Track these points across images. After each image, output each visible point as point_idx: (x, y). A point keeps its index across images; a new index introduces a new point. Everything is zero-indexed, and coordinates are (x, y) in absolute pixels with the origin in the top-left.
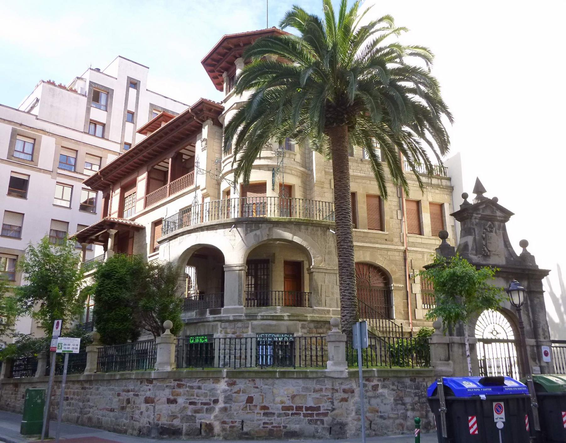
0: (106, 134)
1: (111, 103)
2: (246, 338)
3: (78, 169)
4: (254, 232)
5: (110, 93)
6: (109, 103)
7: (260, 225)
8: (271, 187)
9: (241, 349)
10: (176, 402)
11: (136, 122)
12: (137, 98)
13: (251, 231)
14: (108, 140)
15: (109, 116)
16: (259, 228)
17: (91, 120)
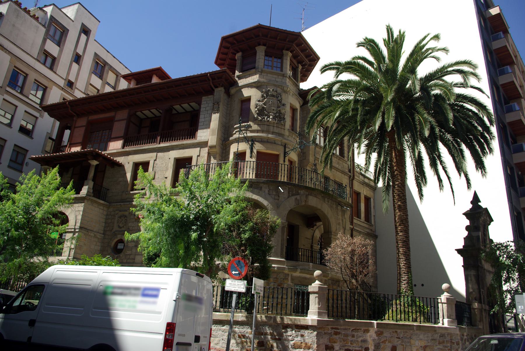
0: (55, 67)
3: (25, 92)
4: (295, 197)
5: (66, 32)
6: (63, 40)
10: (334, 349)
13: (293, 195)
14: (55, 73)
15: (61, 52)
17: (45, 50)
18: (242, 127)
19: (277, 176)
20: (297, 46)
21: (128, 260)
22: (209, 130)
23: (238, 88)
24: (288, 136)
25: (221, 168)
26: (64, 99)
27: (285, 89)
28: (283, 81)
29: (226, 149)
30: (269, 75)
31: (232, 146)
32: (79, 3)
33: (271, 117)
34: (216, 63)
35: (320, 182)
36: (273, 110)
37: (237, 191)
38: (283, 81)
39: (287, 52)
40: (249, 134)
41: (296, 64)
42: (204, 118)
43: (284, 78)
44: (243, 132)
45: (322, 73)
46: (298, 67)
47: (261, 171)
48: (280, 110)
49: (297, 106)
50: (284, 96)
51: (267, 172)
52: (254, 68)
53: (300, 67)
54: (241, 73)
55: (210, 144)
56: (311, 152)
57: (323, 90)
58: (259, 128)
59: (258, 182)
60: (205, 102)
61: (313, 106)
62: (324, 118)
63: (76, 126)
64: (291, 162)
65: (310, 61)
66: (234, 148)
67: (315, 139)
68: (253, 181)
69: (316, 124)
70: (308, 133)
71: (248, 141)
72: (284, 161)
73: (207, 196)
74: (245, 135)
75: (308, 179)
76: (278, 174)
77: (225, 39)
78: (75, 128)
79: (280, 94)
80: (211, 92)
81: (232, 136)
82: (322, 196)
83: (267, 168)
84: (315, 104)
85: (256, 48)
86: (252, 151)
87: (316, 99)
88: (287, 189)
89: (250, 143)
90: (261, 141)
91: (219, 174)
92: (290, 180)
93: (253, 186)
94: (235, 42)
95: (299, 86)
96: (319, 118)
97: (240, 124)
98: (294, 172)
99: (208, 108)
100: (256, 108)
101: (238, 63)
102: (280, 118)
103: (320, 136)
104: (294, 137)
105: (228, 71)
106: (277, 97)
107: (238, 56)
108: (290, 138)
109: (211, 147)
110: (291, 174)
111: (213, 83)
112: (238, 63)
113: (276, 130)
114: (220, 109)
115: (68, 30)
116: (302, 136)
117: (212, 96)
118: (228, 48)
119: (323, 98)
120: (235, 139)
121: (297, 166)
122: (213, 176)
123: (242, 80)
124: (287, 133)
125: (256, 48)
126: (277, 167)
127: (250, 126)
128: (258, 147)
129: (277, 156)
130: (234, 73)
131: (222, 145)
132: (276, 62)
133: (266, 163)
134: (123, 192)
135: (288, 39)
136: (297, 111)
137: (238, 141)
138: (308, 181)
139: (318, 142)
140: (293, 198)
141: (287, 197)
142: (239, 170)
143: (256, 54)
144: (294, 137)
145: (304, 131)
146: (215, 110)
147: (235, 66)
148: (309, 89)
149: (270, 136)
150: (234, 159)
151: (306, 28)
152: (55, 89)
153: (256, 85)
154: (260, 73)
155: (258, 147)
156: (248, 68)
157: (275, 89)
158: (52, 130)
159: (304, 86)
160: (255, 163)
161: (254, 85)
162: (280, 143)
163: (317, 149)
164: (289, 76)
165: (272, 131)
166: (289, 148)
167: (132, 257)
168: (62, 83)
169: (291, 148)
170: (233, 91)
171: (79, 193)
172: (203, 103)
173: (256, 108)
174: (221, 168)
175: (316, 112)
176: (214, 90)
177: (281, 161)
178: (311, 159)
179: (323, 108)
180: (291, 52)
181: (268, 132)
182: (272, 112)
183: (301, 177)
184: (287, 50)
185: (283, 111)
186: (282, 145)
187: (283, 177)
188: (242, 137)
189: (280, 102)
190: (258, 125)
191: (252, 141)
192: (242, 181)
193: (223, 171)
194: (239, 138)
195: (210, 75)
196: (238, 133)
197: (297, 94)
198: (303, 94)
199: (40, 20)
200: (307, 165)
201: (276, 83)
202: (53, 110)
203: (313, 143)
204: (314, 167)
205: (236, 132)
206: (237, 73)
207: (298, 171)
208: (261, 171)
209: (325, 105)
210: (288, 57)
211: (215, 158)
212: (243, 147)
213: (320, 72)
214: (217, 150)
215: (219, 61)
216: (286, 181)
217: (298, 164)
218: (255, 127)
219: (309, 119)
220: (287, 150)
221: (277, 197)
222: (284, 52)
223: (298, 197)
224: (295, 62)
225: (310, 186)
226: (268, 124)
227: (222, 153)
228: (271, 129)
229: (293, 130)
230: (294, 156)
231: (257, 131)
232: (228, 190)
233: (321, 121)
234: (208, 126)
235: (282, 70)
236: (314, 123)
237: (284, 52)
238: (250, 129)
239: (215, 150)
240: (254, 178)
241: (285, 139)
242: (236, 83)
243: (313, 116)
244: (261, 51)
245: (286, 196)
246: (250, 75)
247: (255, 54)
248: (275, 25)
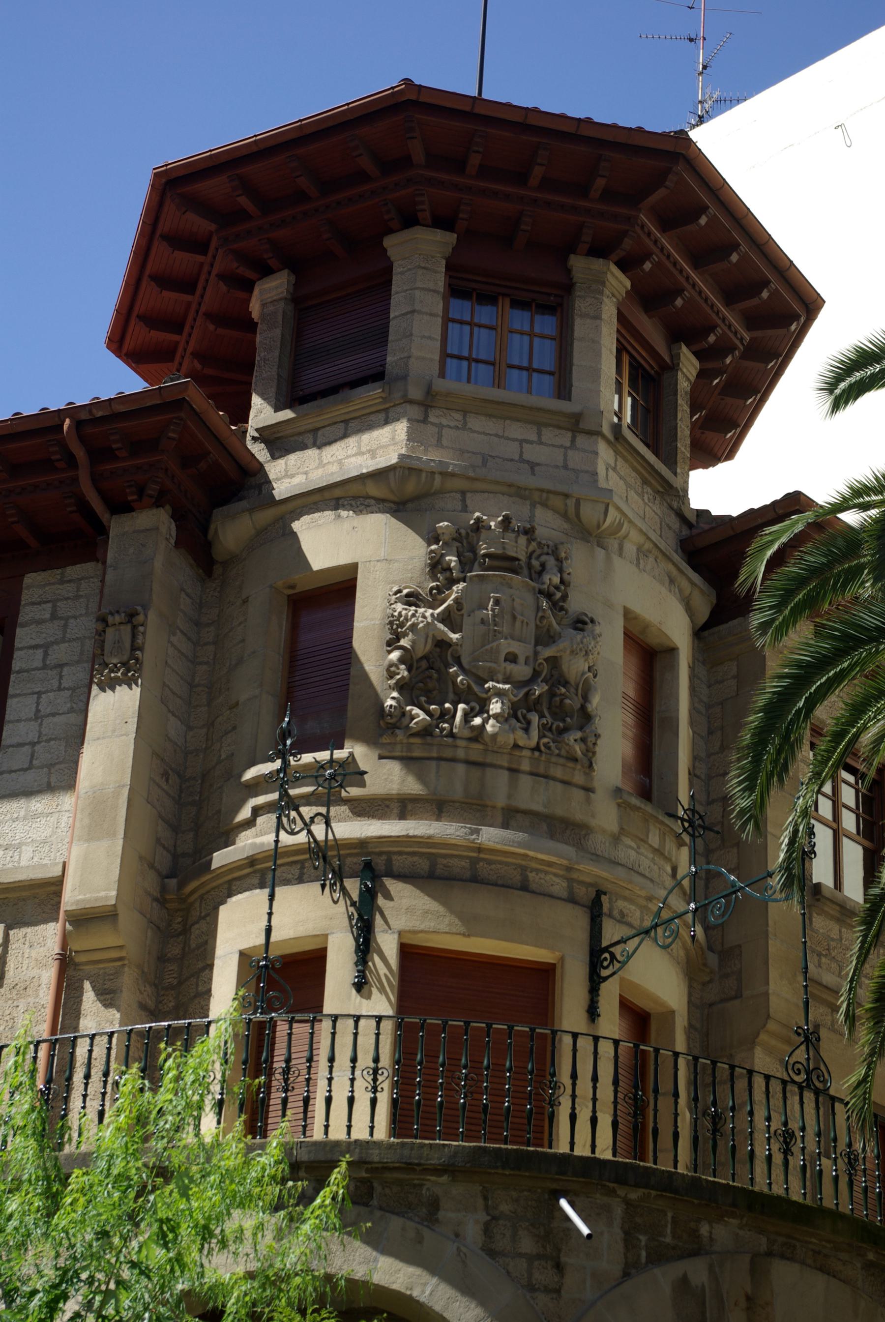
4: (677, 1269)
13: (658, 1257)
18: (298, 781)
19: (541, 1121)
20: (667, 224)
22: (67, 801)
23: (265, 516)
24: (616, 839)
25: (152, 1073)
27: (590, 513)
28: (575, 459)
29: (186, 931)
30: (476, 423)
31: (225, 913)
33: (495, 707)
34: (118, 342)
35: (852, 1160)
36: (512, 658)
37: (268, 1239)
38: (575, 459)
39: (597, 264)
40: (349, 828)
41: (661, 348)
42: (38, 716)
43: (582, 441)
44: (307, 811)
45: (838, 404)
46: (672, 367)
47: (429, 1087)
48: (554, 662)
49: (676, 627)
50: (580, 562)
51: (473, 1092)
52: (378, 376)
53: (689, 366)
54: (287, 414)
55: (72, 897)
56: (780, 948)
57: (852, 518)
58: (413, 786)
59: (409, 1167)
60: (45, 611)
61: (782, 630)
62: (858, 710)
64: (639, 1019)
65: (752, 321)
66: (239, 927)
67: (800, 853)
68: (375, 1156)
69: (806, 754)
70: (756, 816)
71: (339, 876)
72: (593, 1012)
73: (51, 1274)
74: (319, 830)
75: (760, 1137)
76: (554, 1103)
77: (175, 187)
79: (554, 552)
80: (82, 541)
81: (227, 838)
82: (869, 1266)
83: (475, 1065)
84: (796, 613)
85: (388, 242)
86: (365, 947)
87: (801, 582)
88: (619, 1211)
89: (353, 886)
90: (432, 871)
91: (141, 1120)
92: (638, 1149)
93: (381, 1193)
94: (244, 201)
95: (682, 495)
96: (830, 711)
97: (283, 755)
98: (665, 1086)
99: (60, 653)
100: (392, 644)
101: (269, 347)
102: (559, 711)
103: (837, 835)
104: (654, 839)
105: (197, 397)
106: (536, 567)
107: (269, 295)
108: (628, 852)
109: (84, 920)
110: (639, 1108)
111: (95, 480)
112: (269, 347)
113: (531, 796)
114: (148, 657)
116: (708, 829)
118: (197, 245)
119: (854, 574)
120: (252, 861)
121: (680, 1046)
122: (96, 1127)
123: (293, 459)
124: (605, 816)
125: (388, 242)
126: (541, 1051)
127: (350, 772)
128: (409, 913)
129: (543, 976)
130: (241, 414)
131: (161, 901)
132: (525, 335)
133: (468, 1025)
135: (600, 183)
136: (673, 666)
137: (267, 871)
138: (761, 1151)
139: (821, 871)
140: (664, 1277)
142: (278, 1079)
143: (388, 283)
144: (654, 839)
145: (726, 800)
146: (111, 661)
147: (248, 366)
148: (750, 514)
149: (491, 836)
150: (244, 1004)
151: (726, 103)
153: (391, 493)
154: (415, 411)
155: (409, 913)
156: (335, 377)
157: (520, 513)
159: (719, 491)
160: (387, 1027)
161: (372, 489)
162: (559, 887)
163: (819, 922)
164: (617, 429)
165: (501, 801)
166: (622, 920)
169: (639, 918)
170: (232, 531)
172: (26, 613)
173: (392, 644)
174: (152, 1073)
175: (803, 675)
176: (102, 530)
177: (571, 1013)
178: (782, 993)
179: (849, 641)
180: (624, 266)
181: (475, 808)
182: (500, 676)
183: (713, 1127)
184: (599, 251)
185: (575, 667)
186: (572, 900)
187: (586, 1130)
188: (296, 850)
189: (558, 606)
190: (407, 761)
191: (364, 874)
192: (304, 1156)
193: (164, 1096)
194: (277, 851)
195: (78, 425)
196: (267, 821)
197: (668, 544)
198: (714, 549)
200: (751, 1042)
201: (531, 482)
203: (787, 885)
204: (800, 1055)
205: (257, 811)
206: (262, 412)
207: (694, 1083)
208: (429, 1087)
209: (870, 620)
210: (604, 302)
211: (107, 997)
212: (306, 913)
213: (828, 401)
214: (127, 938)
215: (139, 334)
216: (605, 1153)
217: (691, 1028)
218: (385, 776)
219: (754, 719)
220: (611, 933)
221: (543, 1275)
222: (579, 264)
223: (697, 1271)
224: (652, 331)
225: (778, 1190)
226: (480, 755)
227: (162, 959)
228: (499, 788)
229: (646, 794)
230: (657, 976)
231: (402, 806)
232: (205, 1233)
233: (838, 736)
234: (59, 775)
235: (563, 391)
236: (789, 746)
237: (579, 264)
238: (354, 791)
239: (110, 940)
240: (381, 1133)
241: (596, 857)
242: (248, 481)
243: (784, 698)
244: (418, 264)
245: (610, 1262)
246: (348, 428)
247: (381, 281)
248: (515, 85)
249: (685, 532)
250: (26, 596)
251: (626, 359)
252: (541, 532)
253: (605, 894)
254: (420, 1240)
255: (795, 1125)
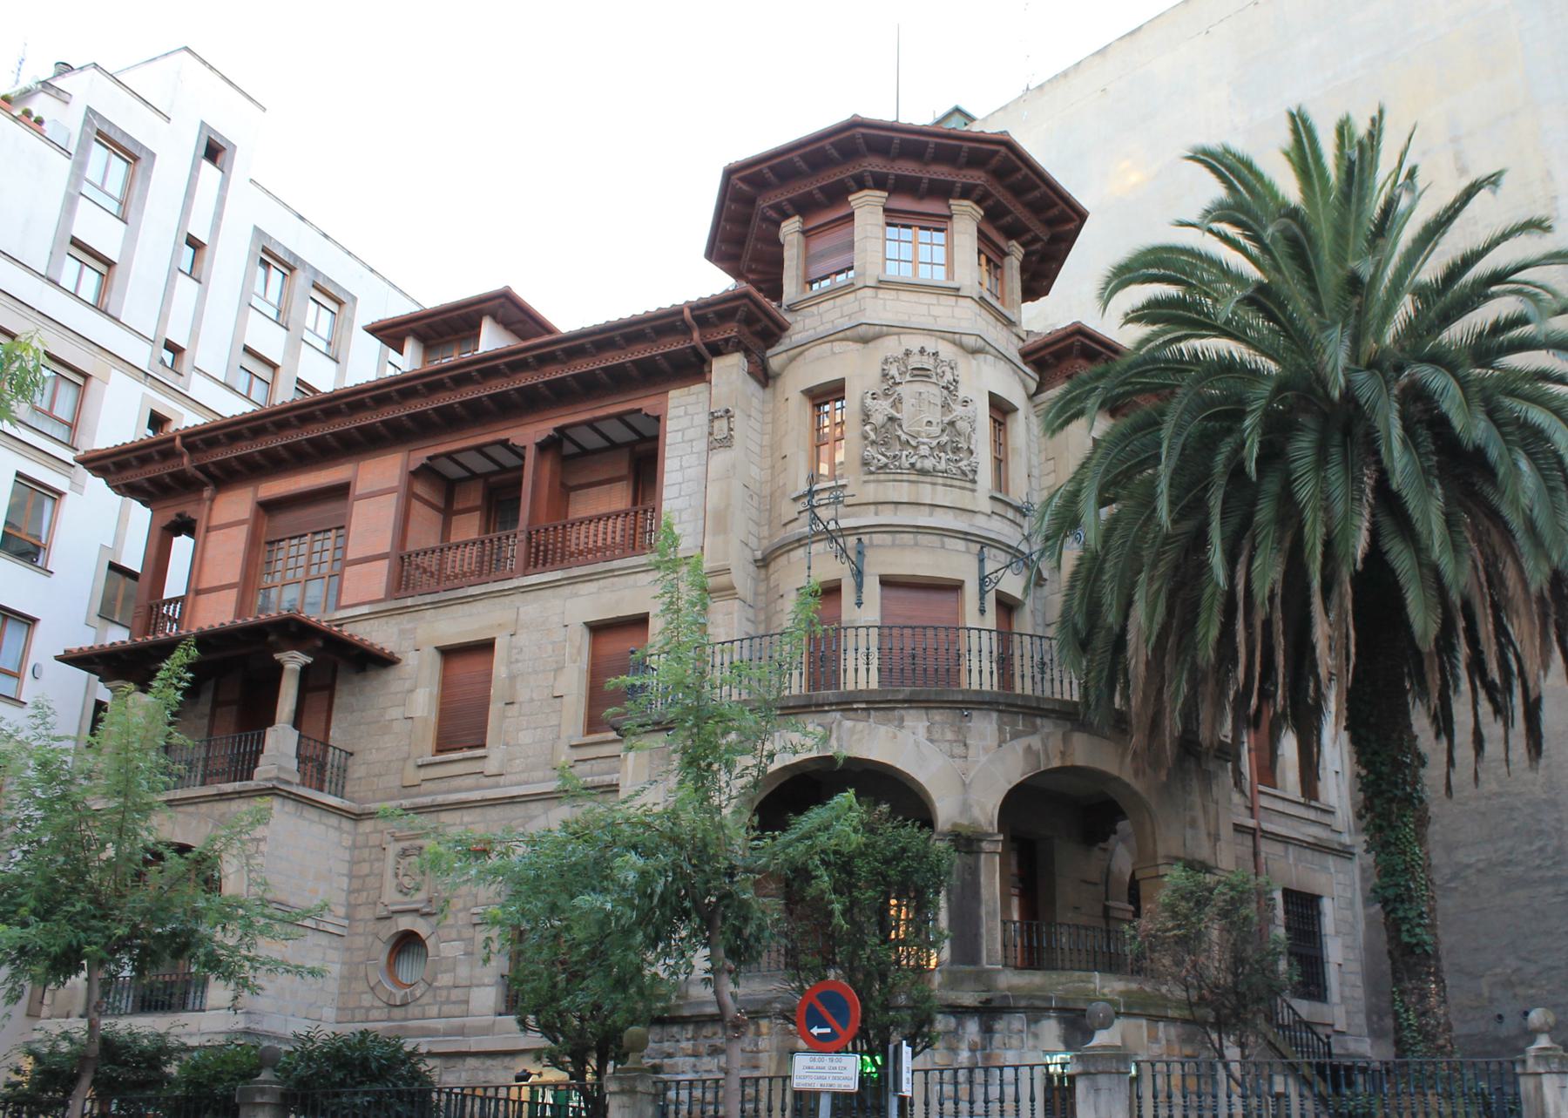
1: (143, 197)
2: (1016, 1068)
7: (1038, 721)
8: (977, 605)
9: (1002, 1101)
11: (209, 278)
12: (221, 201)
13: (1016, 736)
14: (117, 320)
15: (130, 241)
16: (1034, 730)
21: (445, 1009)
26: (157, 421)
32: (187, 49)
60: (681, 411)
63: (214, 522)
65: (1050, 223)
77: (730, 173)
78: (208, 530)
99: (690, 434)
115: (154, 155)
117: (699, 388)
134: (405, 760)
141: (996, 744)
152: (118, 378)
158: (119, 538)
167: (456, 994)
168: (142, 355)
171: (250, 777)
199: (47, 127)
202: (114, 467)
249: (1021, 344)
250: (671, 404)
251: (983, 258)
252: (942, 356)
253: (228, 976)
254: (895, 737)
255: (1047, 660)
